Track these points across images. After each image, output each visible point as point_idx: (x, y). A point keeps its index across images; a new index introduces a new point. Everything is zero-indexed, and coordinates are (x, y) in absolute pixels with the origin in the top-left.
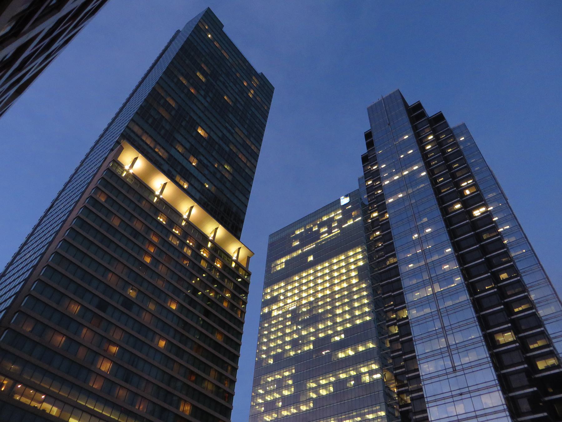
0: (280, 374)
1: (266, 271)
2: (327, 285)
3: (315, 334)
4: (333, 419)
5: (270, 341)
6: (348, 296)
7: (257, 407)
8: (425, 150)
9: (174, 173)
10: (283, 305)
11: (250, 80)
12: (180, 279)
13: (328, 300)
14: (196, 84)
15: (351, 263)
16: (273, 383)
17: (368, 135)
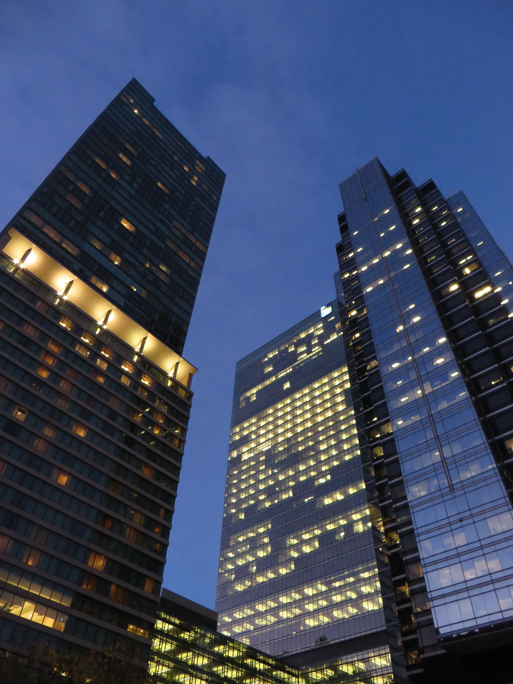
0: (252, 531)
1: (234, 407)
2: (308, 416)
3: (294, 478)
4: (319, 582)
5: (240, 491)
6: (333, 427)
7: (227, 575)
8: (411, 225)
9: (89, 273)
10: (255, 445)
11: (192, 165)
12: (90, 399)
13: (310, 434)
14: (119, 167)
15: (336, 386)
16: (244, 544)
17: (342, 219)
